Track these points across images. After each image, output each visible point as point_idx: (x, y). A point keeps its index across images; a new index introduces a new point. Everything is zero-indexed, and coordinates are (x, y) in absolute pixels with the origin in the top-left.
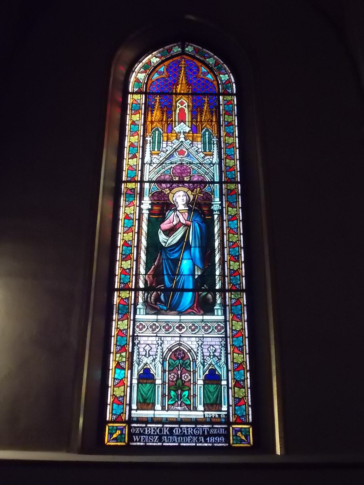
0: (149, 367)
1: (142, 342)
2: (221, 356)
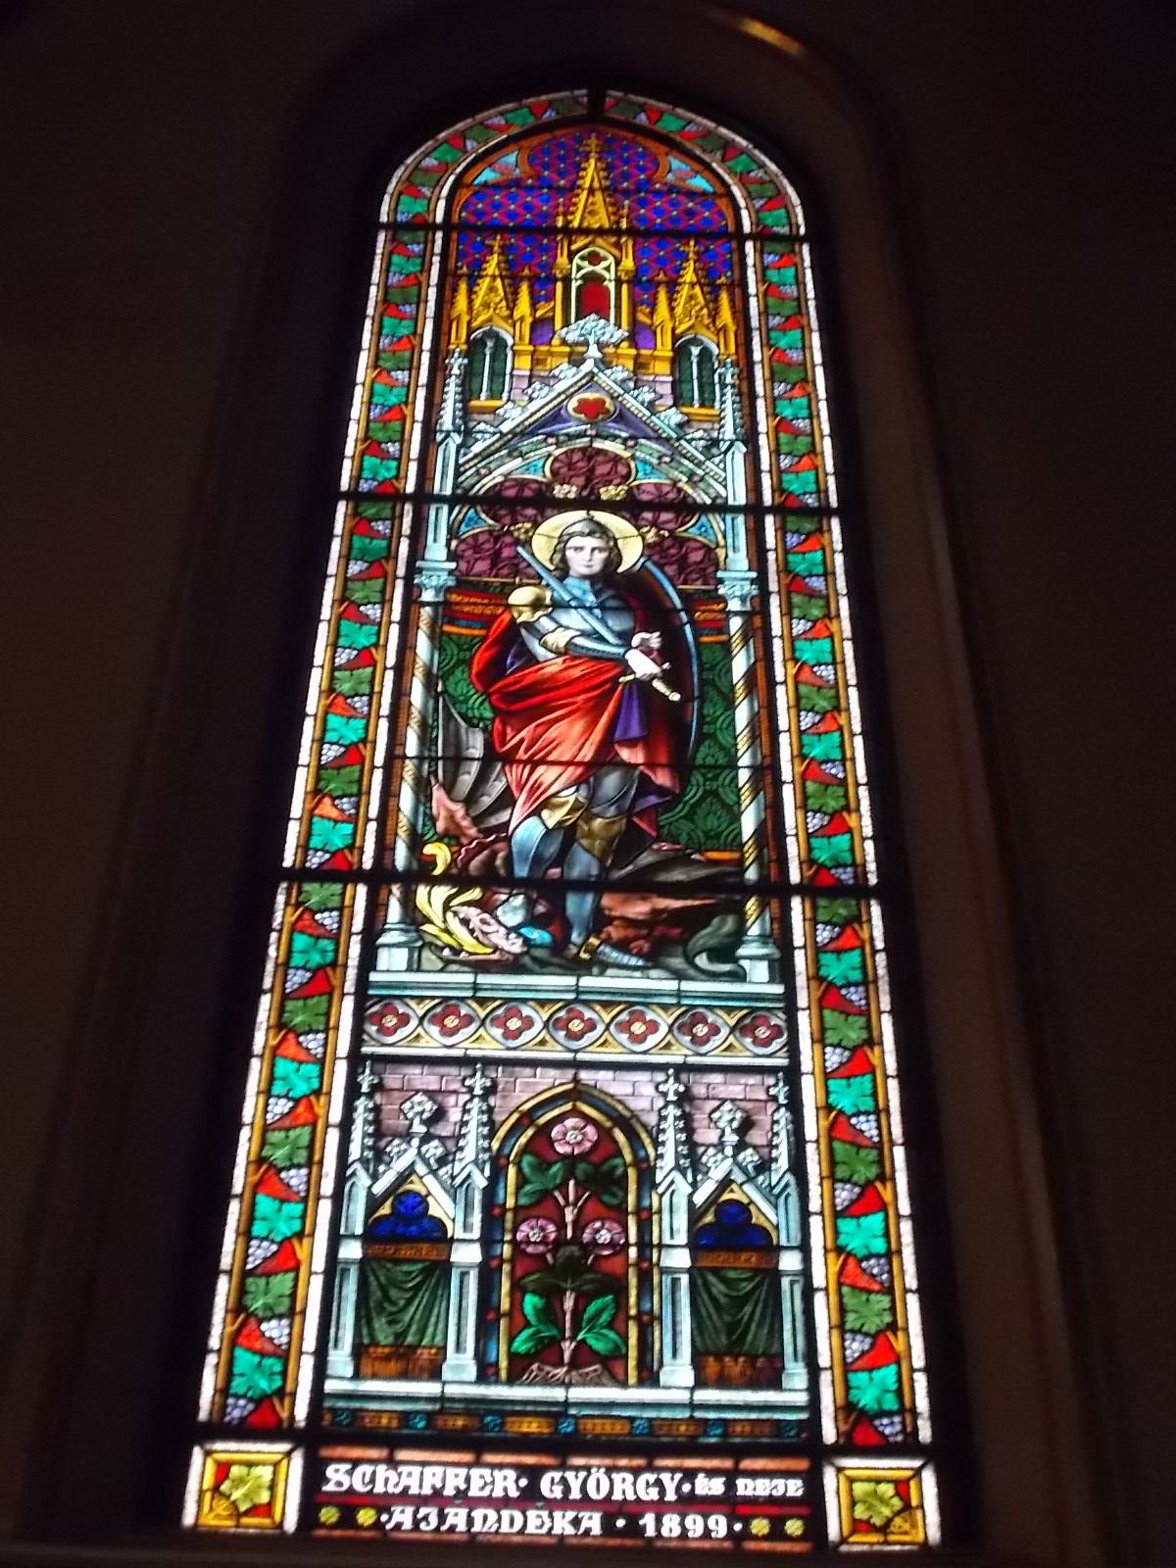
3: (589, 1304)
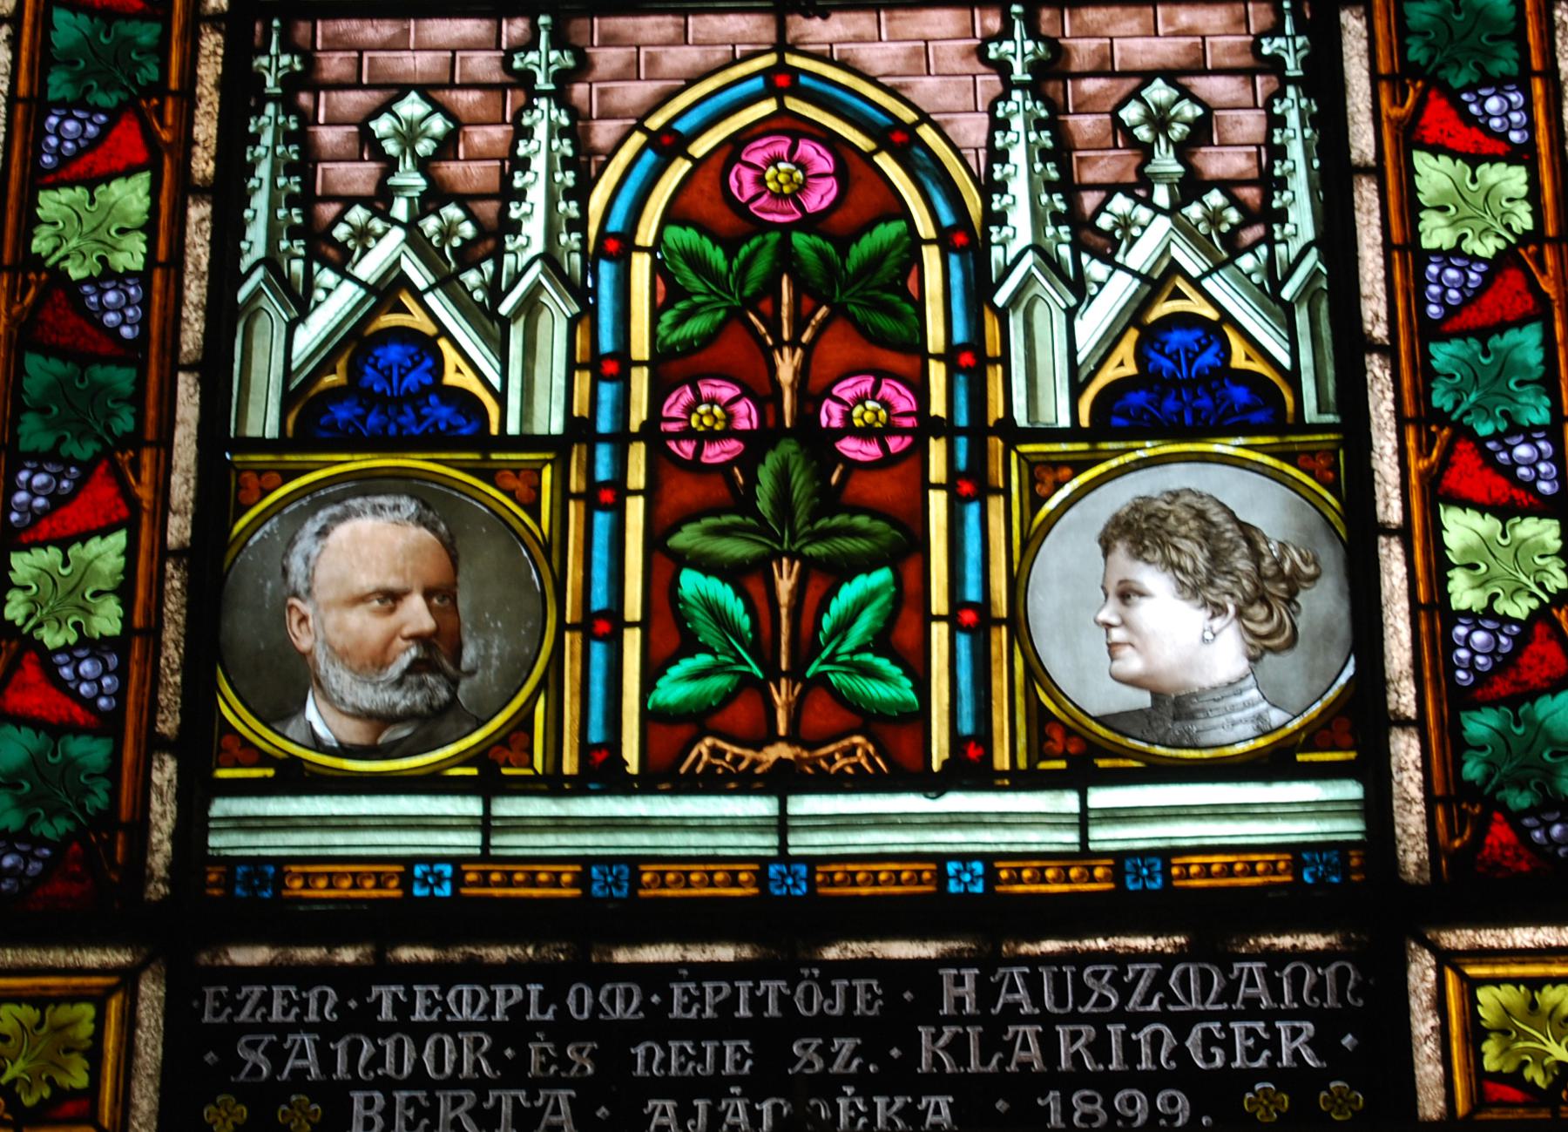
0: (417, 320)
1: (335, 65)
2: (1270, 183)
3: (833, 592)
